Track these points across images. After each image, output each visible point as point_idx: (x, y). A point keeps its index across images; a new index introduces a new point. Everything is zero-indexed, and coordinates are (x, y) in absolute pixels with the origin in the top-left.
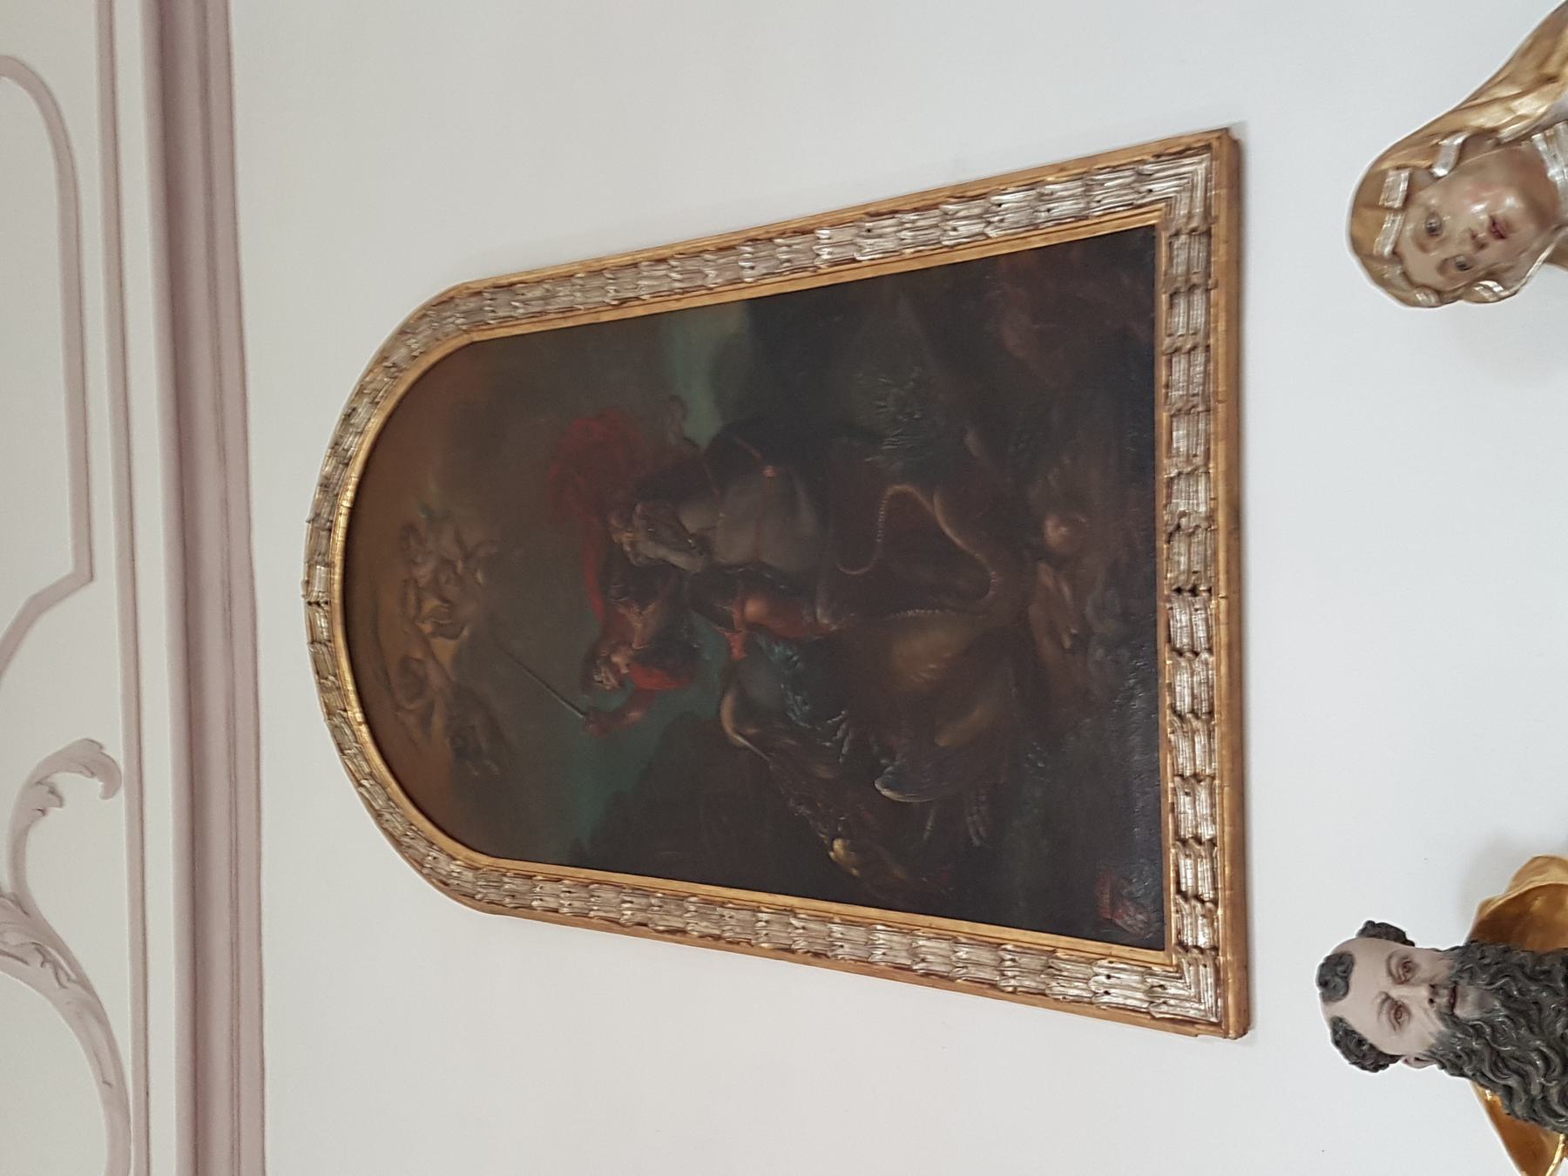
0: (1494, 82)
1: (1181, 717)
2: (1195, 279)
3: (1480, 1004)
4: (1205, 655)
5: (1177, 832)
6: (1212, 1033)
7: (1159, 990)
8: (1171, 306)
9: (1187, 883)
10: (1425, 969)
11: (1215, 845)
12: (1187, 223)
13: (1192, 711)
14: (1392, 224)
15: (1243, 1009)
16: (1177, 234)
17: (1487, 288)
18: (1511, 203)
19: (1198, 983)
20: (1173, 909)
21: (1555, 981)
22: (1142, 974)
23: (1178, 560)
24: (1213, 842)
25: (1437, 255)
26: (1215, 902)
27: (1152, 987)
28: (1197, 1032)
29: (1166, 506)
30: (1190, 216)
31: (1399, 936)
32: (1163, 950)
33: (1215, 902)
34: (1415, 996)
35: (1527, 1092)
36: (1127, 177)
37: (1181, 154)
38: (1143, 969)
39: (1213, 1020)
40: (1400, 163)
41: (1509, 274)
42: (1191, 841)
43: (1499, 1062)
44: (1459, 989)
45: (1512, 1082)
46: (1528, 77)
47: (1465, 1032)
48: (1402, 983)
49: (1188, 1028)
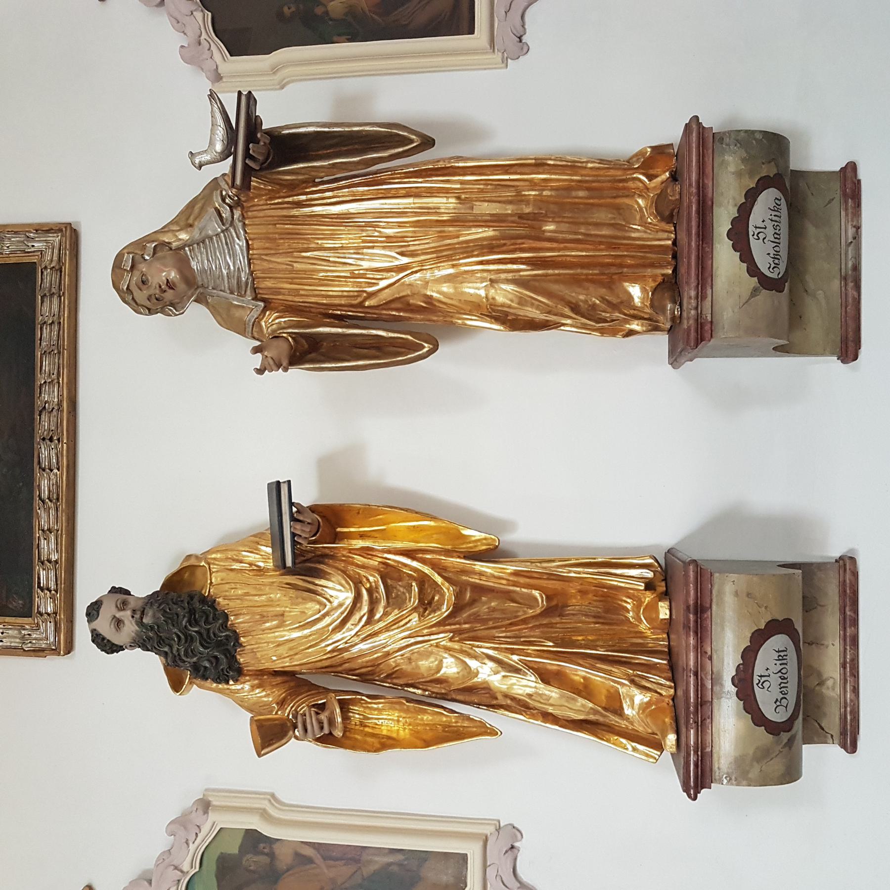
0: (171, 223)
1: (43, 501)
2: (53, 290)
3: (154, 616)
4: (55, 471)
5: (39, 558)
6: (53, 654)
7: (28, 636)
8: (42, 302)
9: (43, 582)
10: (132, 604)
11: (57, 563)
12: (50, 264)
13: (49, 498)
14: (127, 277)
15: (68, 641)
16: (46, 268)
17: (171, 310)
18: (173, 275)
19: (46, 631)
20: (36, 596)
21: (184, 604)
22: (19, 630)
23: (45, 424)
24: (56, 562)
25: (146, 293)
26: (56, 591)
27: (25, 635)
28: (45, 655)
29: (39, 398)
30: (52, 261)
31: (127, 593)
32: (31, 617)
33: (56, 591)
34: (126, 615)
35: (172, 652)
36: (22, 238)
37: (49, 231)
38: (19, 627)
39: (54, 648)
40: (130, 251)
41: (180, 305)
42: (46, 562)
43: (161, 641)
44: (146, 611)
45: (166, 649)
46: (182, 223)
47: (147, 629)
48: (122, 610)
49: (41, 654)
